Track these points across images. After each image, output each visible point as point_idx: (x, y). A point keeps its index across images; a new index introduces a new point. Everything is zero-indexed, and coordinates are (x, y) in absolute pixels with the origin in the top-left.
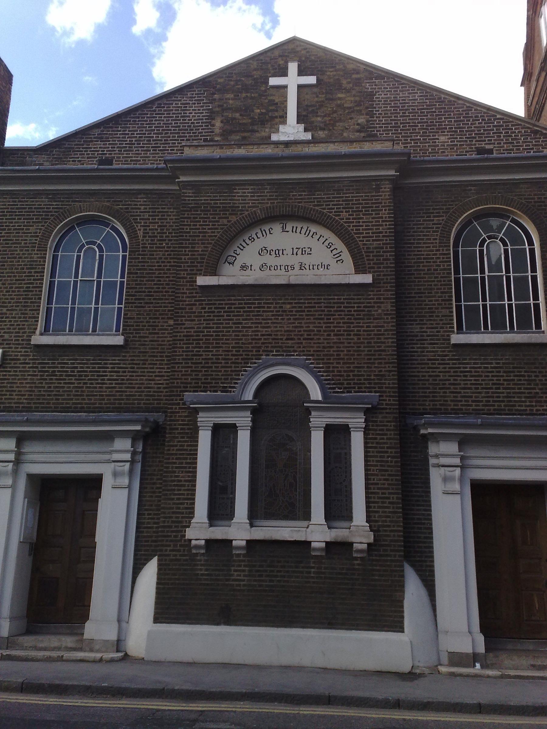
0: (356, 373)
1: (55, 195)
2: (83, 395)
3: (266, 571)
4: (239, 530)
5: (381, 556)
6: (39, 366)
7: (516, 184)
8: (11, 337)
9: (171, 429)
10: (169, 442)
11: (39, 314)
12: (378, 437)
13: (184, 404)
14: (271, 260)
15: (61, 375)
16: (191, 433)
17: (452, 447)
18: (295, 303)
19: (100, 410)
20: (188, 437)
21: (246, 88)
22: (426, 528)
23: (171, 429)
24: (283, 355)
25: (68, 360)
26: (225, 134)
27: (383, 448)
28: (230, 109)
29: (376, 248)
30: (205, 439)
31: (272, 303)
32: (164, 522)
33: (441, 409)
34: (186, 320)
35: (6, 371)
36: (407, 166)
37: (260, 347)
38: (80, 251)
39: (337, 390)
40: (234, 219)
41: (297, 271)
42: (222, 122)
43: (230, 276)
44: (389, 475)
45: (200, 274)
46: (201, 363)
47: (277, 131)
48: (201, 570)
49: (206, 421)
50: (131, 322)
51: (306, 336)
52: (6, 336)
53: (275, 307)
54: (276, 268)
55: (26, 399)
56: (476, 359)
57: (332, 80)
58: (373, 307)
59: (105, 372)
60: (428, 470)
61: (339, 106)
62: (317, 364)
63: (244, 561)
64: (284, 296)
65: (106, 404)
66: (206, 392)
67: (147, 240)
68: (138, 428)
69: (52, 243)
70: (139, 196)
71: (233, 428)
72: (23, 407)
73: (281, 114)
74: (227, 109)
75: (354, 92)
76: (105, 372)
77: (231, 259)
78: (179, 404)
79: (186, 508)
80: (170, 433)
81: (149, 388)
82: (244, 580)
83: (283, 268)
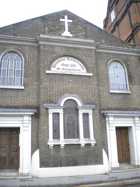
4: (62, 142)
5: (98, 146)
7: (121, 55)
13: (44, 107)
14: (65, 67)
15: (5, 97)
30: (81, 117)
37: (64, 91)
38: (9, 60)
40: (55, 55)
41: (72, 71)
43: (53, 70)
47: (63, 33)
49: (51, 111)
60: (106, 124)
69: (3, 53)
71: (58, 114)
78: (42, 107)
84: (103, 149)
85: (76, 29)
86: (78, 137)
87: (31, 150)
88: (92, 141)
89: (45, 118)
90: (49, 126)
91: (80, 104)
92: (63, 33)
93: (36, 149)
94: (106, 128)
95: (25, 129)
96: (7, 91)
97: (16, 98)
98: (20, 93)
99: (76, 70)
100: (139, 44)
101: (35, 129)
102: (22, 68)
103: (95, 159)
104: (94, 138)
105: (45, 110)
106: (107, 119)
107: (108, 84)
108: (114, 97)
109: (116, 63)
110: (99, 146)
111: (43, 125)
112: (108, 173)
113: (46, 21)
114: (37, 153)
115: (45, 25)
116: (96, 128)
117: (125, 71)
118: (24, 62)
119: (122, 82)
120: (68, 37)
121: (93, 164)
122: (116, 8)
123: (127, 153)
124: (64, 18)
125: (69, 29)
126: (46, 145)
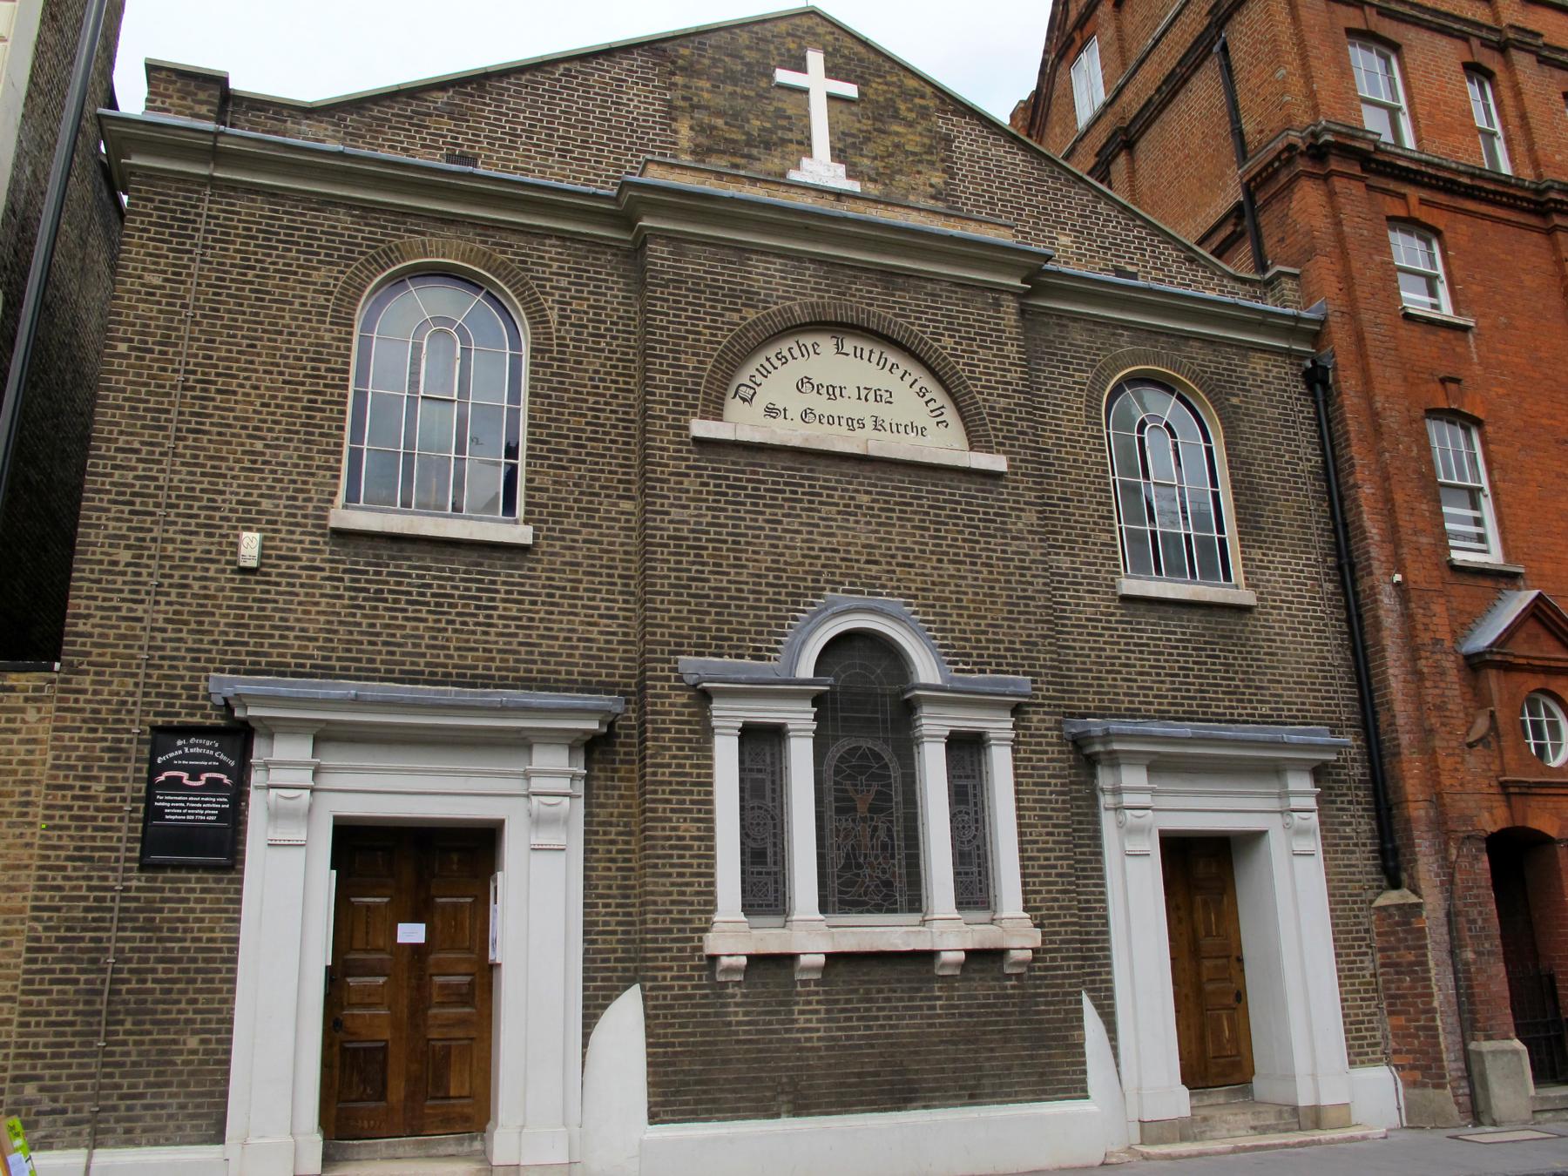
0: (990, 636)
2: (448, 648)
3: (858, 1010)
4: (810, 932)
6: (346, 576)
8: (277, 506)
9: (656, 730)
10: (652, 756)
11: (339, 461)
12: (1034, 756)
13: (680, 679)
14: (821, 405)
15: (396, 601)
16: (698, 741)
18: (878, 493)
19: (486, 681)
20: (691, 749)
21: (732, 77)
22: (1098, 917)
23: (656, 730)
24: (862, 592)
25: (410, 567)
27: (1042, 776)
28: (707, 108)
29: (1005, 410)
30: (933, 764)
31: (835, 489)
32: (655, 921)
33: (1110, 709)
34: (672, 505)
35: (268, 583)
37: (820, 573)
39: (961, 666)
40: (751, 315)
42: (692, 128)
43: (741, 423)
44: (1055, 826)
45: (694, 414)
46: (707, 596)
47: (797, 167)
48: (736, 1014)
49: (728, 716)
50: (539, 497)
51: (900, 560)
53: (842, 497)
54: (831, 420)
55: (319, 648)
56: (1154, 624)
57: (881, 99)
58: (1009, 516)
59: (493, 599)
60: (1096, 815)
61: (897, 146)
62: (925, 614)
63: (817, 993)
64: (857, 477)
65: (498, 669)
66: (721, 656)
67: (567, 332)
68: (594, 725)
70: (547, 242)
71: (777, 734)
72: (312, 666)
73: (798, 136)
74: (699, 107)
75: (919, 128)
76: (493, 599)
78: (668, 679)
79: (698, 893)
80: (655, 739)
81: (588, 640)
82: (818, 1030)
83: (843, 422)
84: (1085, 998)
85: (881, 145)
86: (913, 900)
87: (585, 988)
88: (1013, 927)
89: (687, 757)
90: (712, 821)
91: (926, 668)
92: (797, 167)
93: (616, 988)
94: (1096, 837)
95: (545, 838)
96: (409, 559)
97: (478, 607)
98: (503, 574)
99: (896, 428)
100: (1294, 276)
101: (612, 842)
102: (514, 397)
103: (1031, 1057)
104: (1026, 910)
105: (685, 705)
106: (1104, 779)
107: (1105, 537)
108: (1150, 626)
109: (1151, 395)
110: (1060, 968)
111: (673, 811)
112: (1126, 1157)
113: (678, 79)
114: (627, 1013)
115: (676, 108)
116: (1036, 842)
117: (1209, 451)
118: (533, 350)
119: (1195, 529)
120: (839, 195)
121: (737, 1110)
122: (1119, 29)
123: (1231, 1019)
124: (800, 66)
125: (840, 145)
126: (691, 958)
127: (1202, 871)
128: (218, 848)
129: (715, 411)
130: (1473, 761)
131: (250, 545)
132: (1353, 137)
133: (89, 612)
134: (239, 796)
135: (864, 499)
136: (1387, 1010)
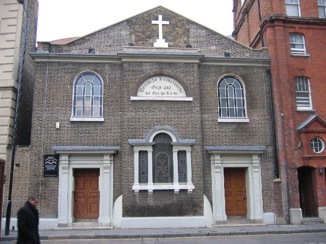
1: (74, 64)
4: (151, 186)
14: (156, 91)
17: (66, 158)
26: (136, 41)
30: (175, 156)
36: (202, 59)
43: (142, 96)
49: (137, 150)
52: (60, 118)
68: (113, 152)
71: (146, 152)
77: (142, 90)
88: (190, 186)
91: (174, 140)
106: (212, 158)
124: (157, 19)
127: (235, 176)
128: (55, 173)
129: (135, 94)
130: (296, 153)
131: (58, 125)
132: (280, 17)
133: (33, 138)
134: (58, 165)
135: (163, 108)
136: (272, 200)
